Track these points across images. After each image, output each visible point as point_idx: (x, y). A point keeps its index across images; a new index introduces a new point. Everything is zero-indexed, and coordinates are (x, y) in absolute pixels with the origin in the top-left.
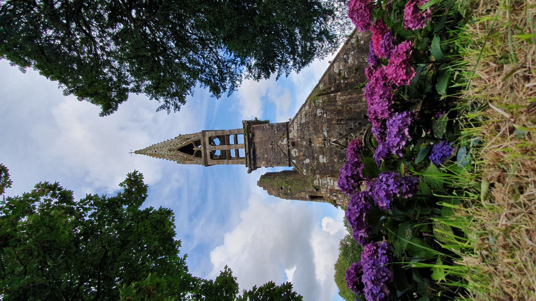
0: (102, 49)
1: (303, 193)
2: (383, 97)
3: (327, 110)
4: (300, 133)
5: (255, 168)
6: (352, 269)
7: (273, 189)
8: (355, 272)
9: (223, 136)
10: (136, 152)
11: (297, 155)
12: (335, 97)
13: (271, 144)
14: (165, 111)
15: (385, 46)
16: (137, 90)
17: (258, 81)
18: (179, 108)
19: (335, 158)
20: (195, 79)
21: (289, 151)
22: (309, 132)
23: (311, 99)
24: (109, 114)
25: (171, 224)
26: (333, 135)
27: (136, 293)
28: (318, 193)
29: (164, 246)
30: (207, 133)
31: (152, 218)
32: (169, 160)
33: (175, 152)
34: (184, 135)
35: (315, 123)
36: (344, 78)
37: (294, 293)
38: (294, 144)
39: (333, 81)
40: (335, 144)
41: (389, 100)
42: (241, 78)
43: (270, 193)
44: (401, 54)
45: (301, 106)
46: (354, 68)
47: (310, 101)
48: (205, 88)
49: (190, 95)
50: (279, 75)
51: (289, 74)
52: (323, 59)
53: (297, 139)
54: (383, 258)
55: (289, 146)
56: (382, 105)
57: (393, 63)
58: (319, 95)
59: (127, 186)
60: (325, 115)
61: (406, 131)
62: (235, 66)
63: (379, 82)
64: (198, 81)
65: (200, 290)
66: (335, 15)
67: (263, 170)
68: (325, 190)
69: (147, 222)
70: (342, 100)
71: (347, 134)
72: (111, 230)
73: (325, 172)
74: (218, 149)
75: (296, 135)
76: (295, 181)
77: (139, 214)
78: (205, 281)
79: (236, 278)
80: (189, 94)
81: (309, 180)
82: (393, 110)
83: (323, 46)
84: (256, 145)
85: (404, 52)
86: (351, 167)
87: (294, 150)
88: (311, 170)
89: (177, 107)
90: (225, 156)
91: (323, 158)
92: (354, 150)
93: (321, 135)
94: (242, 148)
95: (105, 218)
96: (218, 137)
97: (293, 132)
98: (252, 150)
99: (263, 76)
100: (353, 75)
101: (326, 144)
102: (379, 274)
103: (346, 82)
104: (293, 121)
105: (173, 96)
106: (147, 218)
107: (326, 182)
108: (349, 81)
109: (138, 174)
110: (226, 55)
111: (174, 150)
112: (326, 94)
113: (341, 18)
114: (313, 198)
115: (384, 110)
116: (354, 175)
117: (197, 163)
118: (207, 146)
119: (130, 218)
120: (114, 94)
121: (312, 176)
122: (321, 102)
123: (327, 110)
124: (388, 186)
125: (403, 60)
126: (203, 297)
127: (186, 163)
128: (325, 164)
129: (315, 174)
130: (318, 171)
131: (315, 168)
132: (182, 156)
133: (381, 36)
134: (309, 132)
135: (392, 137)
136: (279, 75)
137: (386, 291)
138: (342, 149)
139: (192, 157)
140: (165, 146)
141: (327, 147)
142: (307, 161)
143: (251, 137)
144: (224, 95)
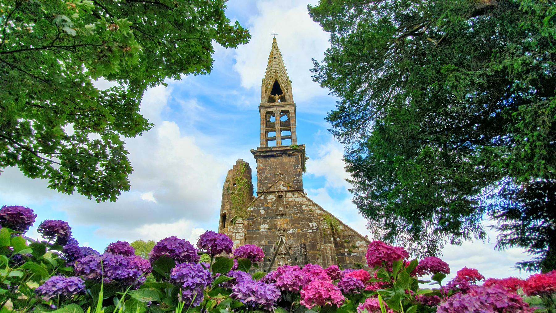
0: (375, 8)
1: (228, 207)
2: (297, 279)
3: (315, 233)
4: (292, 203)
5: (256, 157)
6: (128, 248)
7: (234, 175)
8: (124, 251)
9: (289, 125)
10: (275, 39)
11: (269, 201)
12: (330, 242)
13: (280, 174)
14: (313, 67)
15: (348, 282)
16: (333, 39)
17: (343, 160)
18: (316, 81)
19: (264, 242)
20: (345, 96)
21: (273, 192)
22: (293, 213)
23: (326, 216)
24: (310, 14)
25: (198, 71)
26: (290, 239)
27: (124, 35)
28: (229, 223)
29: (175, 64)
30: (293, 108)
31: (204, 53)
32: (266, 71)
33: (274, 77)
34: (291, 86)
35: (303, 219)
36: (350, 253)
37: (119, 193)
38: (280, 197)
39: (347, 240)
40: (280, 241)
41: (294, 284)
42: (347, 142)
43: (230, 172)
44: (330, 293)
45: (320, 205)
46: (360, 263)
47: (325, 215)
48: (337, 106)
49: (330, 92)
50: (350, 182)
51: (352, 192)
52: (367, 228)
53: (286, 201)
54: (125, 273)
55: (278, 192)
56: (288, 278)
57: (322, 286)
58: (331, 225)
59: (236, 28)
60: (311, 231)
61: (253, 298)
62: (359, 137)
63: (315, 276)
64: (343, 99)
65: (130, 99)
66: (414, 241)
67: (254, 165)
68: (232, 230)
69: (199, 48)
70: (326, 250)
71: (290, 255)
72: (192, 12)
73: (250, 230)
74: (276, 120)
75: (290, 200)
76: (241, 198)
77: (207, 39)
78: (139, 104)
79: (141, 134)
80: (330, 91)
81: (242, 213)
82: (283, 289)
83: (380, 228)
84: (280, 158)
85: (330, 296)
86: (225, 244)
87: (274, 198)
88: (253, 216)
89: (317, 79)
90: (269, 126)
91: (265, 228)
92: (251, 252)
93: (289, 227)
94: (277, 144)
95: (205, 9)
96: (289, 120)
97: (293, 196)
98: (275, 154)
99: (348, 165)
100: (353, 262)
101: (280, 232)
102: (109, 269)
103: (346, 254)
104: (305, 197)
105: (329, 75)
106: (203, 47)
107: (240, 231)
108: (347, 258)
109: (248, 39)
110: (370, 127)
111: (276, 75)
112: (333, 232)
113: (411, 248)
114: (224, 217)
115: (284, 280)
116: (217, 247)
117: (262, 98)
118: (280, 108)
119: (203, 31)
120: (330, 18)
121: (246, 216)
122: (325, 227)
123: (315, 233)
124: (193, 277)
125: (322, 294)
126: (123, 102)
127: (263, 87)
128: (259, 230)
129: (249, 219)
130: (251, 223)
131: (255, 220)
132: (270, 83)
133: (363, 278)
134: (293, 213)
135: (248, 284)
136: (350, 182)
137: (92, 275)
138: (275, 249)
139: (269, 93)
140: (280, 67)
141: (277, 233)
142: (262, 212)
143: (288, 153)
144: (329, 125)
